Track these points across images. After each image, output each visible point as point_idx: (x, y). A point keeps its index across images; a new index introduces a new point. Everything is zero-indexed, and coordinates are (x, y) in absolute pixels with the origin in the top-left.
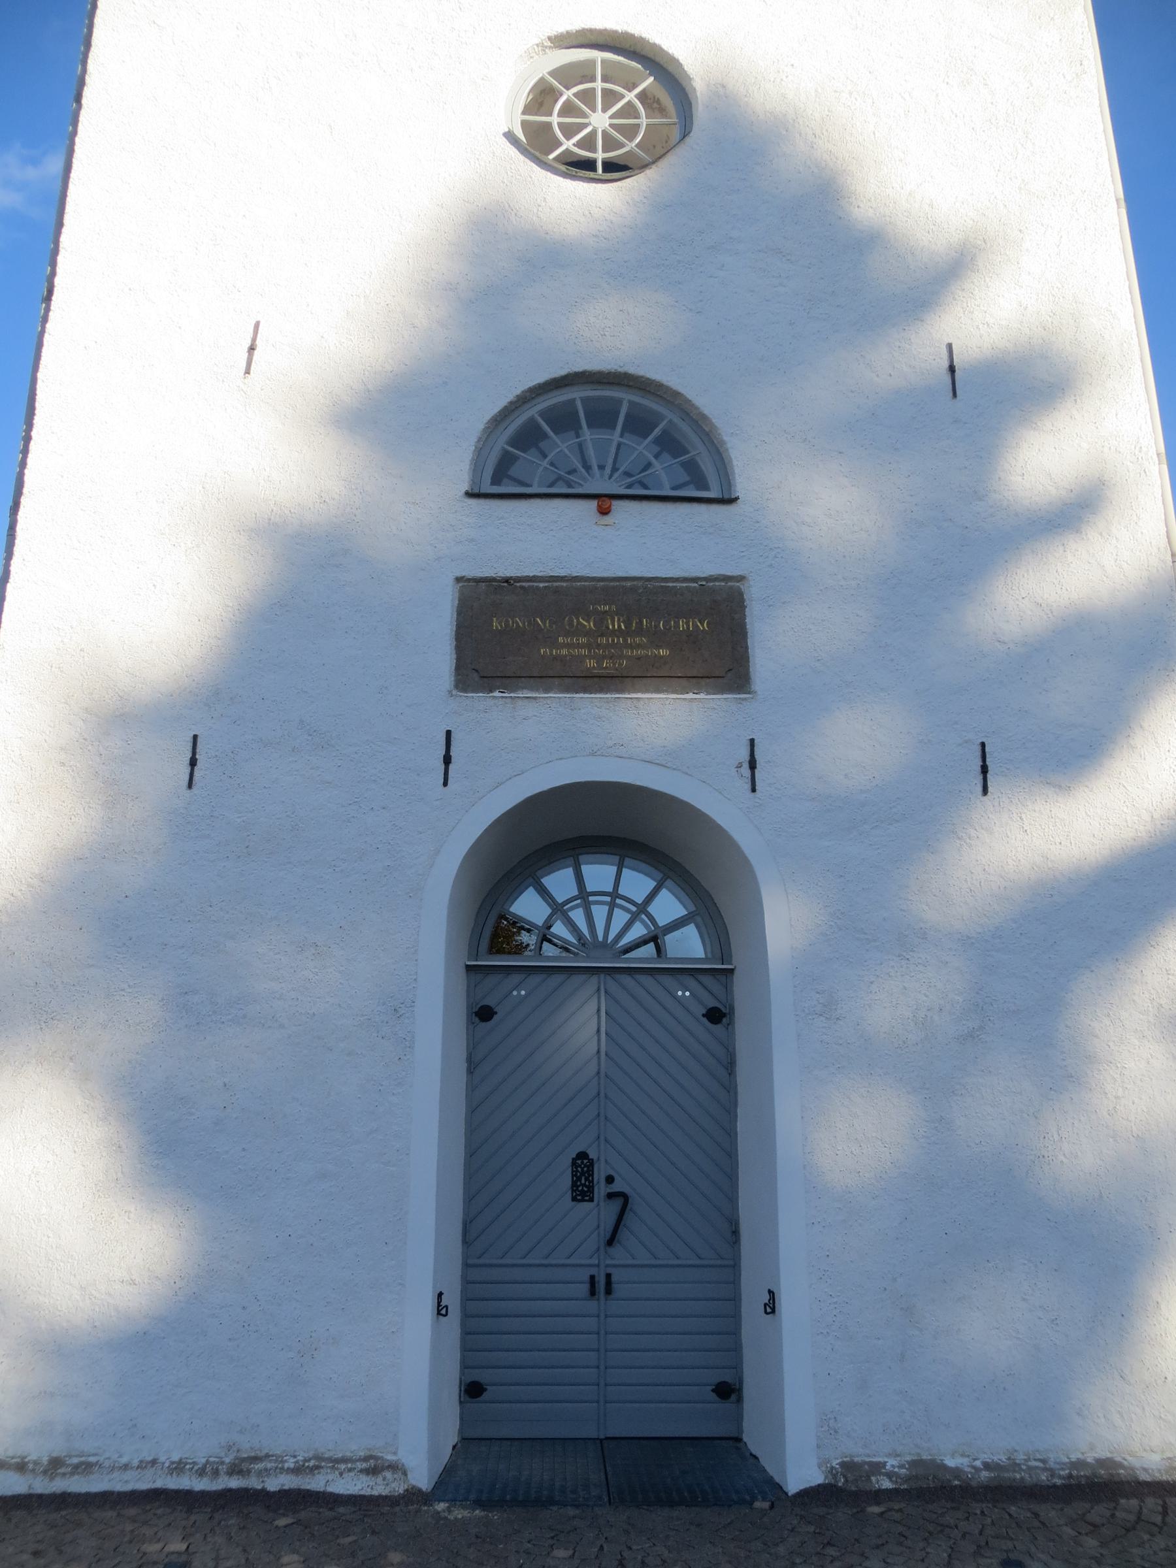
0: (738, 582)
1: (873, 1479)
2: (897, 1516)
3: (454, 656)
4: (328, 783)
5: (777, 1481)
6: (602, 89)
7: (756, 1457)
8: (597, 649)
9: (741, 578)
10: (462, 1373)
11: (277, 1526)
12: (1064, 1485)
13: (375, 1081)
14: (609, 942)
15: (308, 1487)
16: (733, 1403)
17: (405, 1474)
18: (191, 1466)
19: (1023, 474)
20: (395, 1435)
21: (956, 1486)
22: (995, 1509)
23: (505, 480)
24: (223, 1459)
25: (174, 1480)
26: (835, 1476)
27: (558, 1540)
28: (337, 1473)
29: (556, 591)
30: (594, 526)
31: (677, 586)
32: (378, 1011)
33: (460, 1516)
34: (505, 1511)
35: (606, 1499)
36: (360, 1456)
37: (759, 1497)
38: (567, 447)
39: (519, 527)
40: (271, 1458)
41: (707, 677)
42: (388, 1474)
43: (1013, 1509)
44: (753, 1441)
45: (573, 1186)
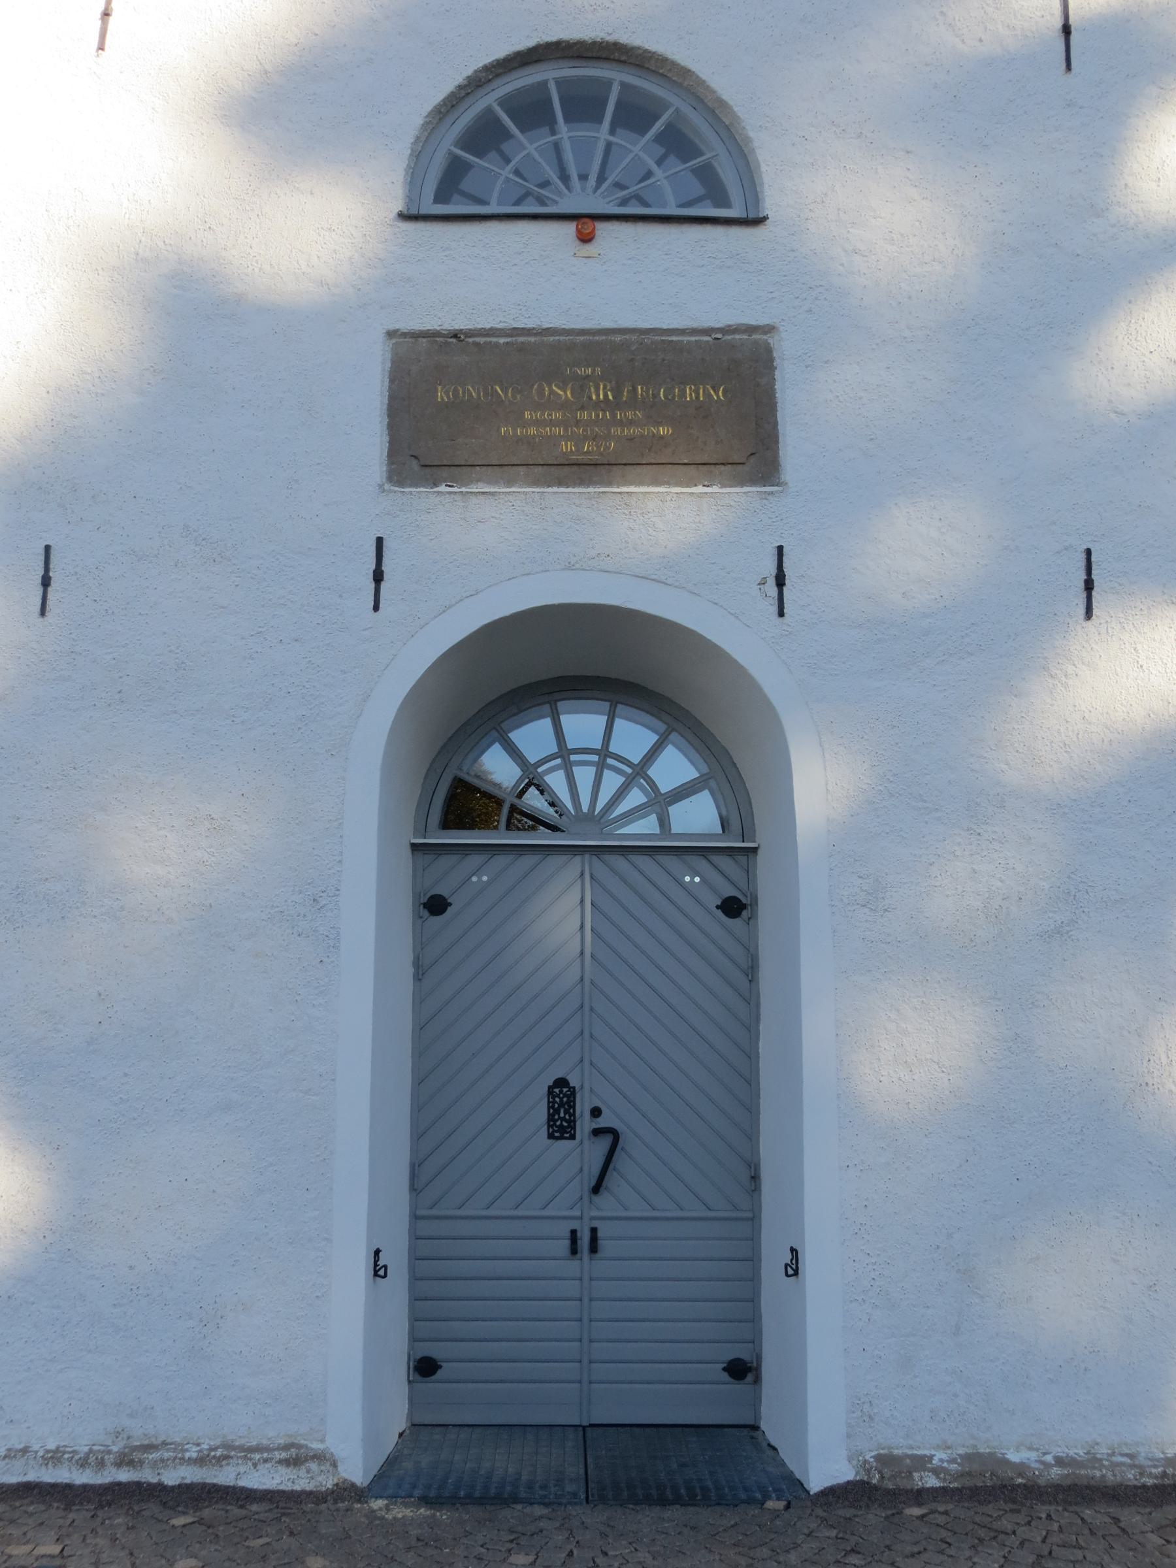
0: (765, 333)
1: (916, 1475)
2: (941, 1519)
3: (386, 438)
4: (223, 608)
5: (798, 1478)
7: (775, 1449)
8: (575, 427)
9: (770, 329)
10: (411, 1348)
11: (173, 1526)
12: (1155, 1486)
13: (290, 989)
14: (596, 813)
15: (215, 1481)
16: (749, 1384)
17: (334, 1465)
18: (71, 1455)
19: (1159, 179)
20: (322, 1419)
21: (1019, 1485)
22: (1065, 1512)
23: (456, 197)
24: (109, 1448)
25: (50, 1471)
26: (868, 1471)
27: (518, 1544)
28: (250, 1464)
29: (522, 349)
30: (573, 258)
31: (683, 341)
32: (292, 902)
33: (400, 1516)
34: (457, 1509)
35: (583, 1496)
36: (280, 1444)
37: (774, 1495)
38: (536, 149)
39: (471, 261)
40: (169, 1446)
41: (723, 464)
42: (313, 1466)
43: (1088, 1513)
44: (772, 1430)
45: (549, 1120)
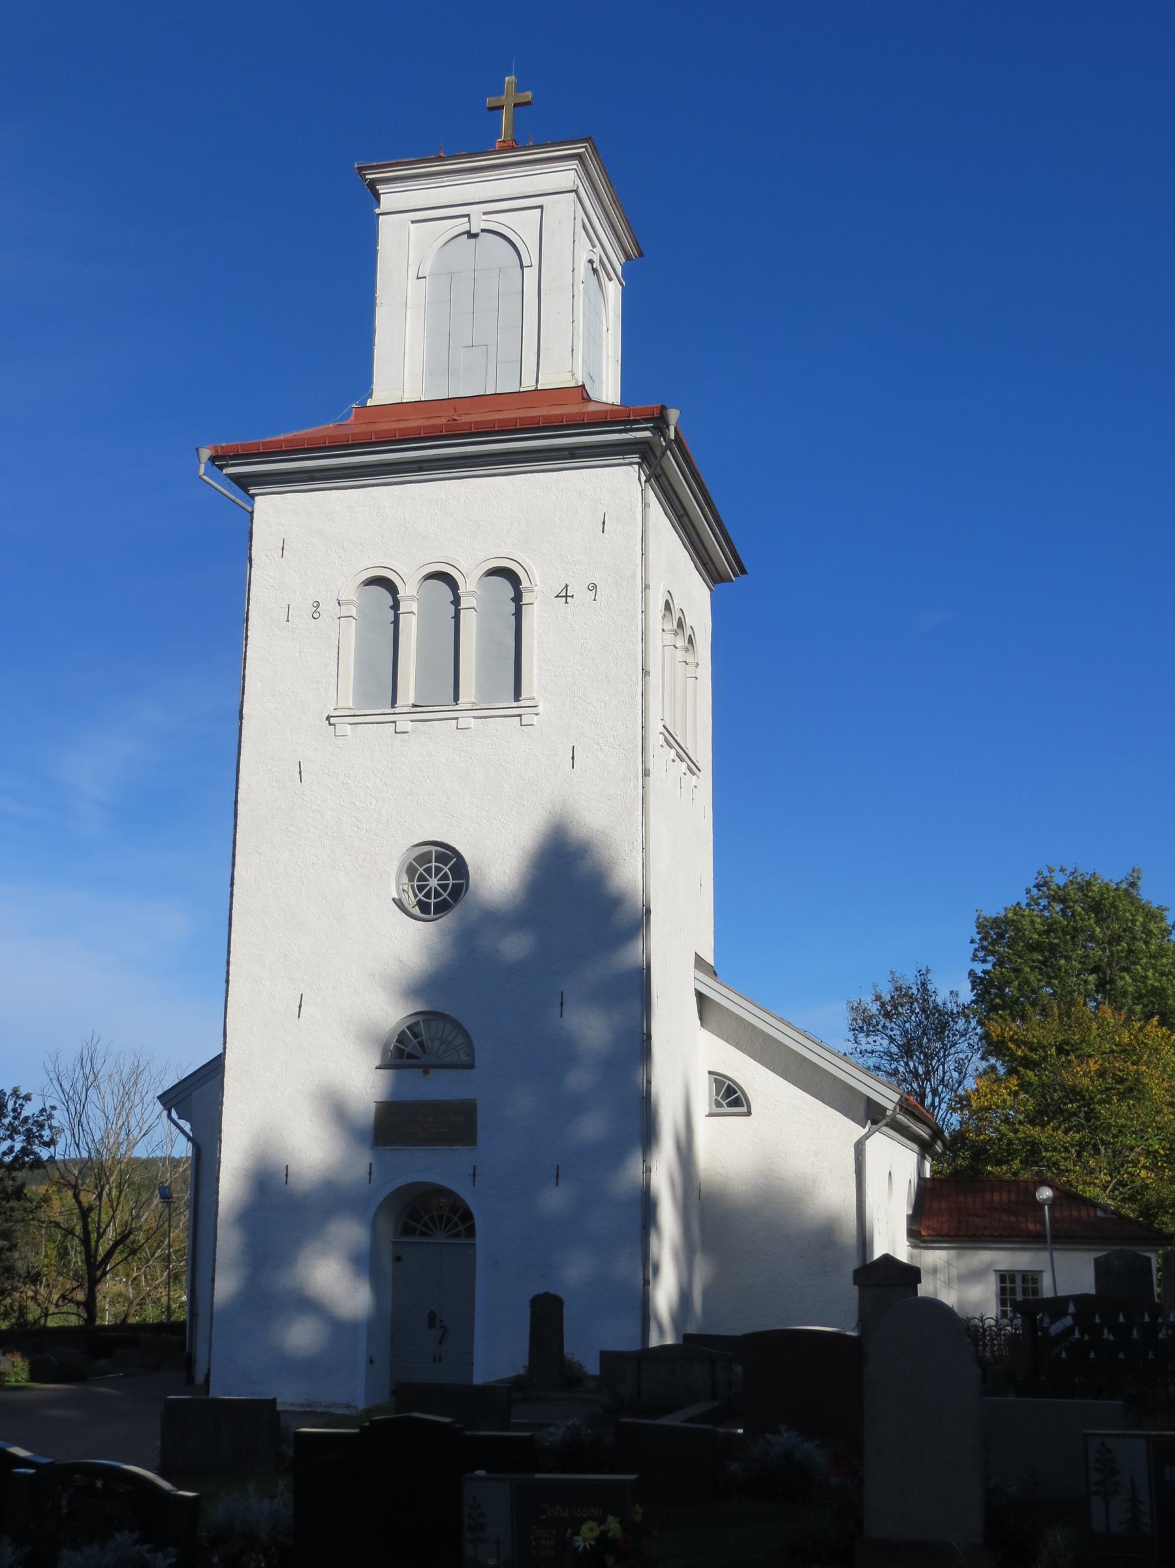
6: (435, 866)
9: (475, 1100)
